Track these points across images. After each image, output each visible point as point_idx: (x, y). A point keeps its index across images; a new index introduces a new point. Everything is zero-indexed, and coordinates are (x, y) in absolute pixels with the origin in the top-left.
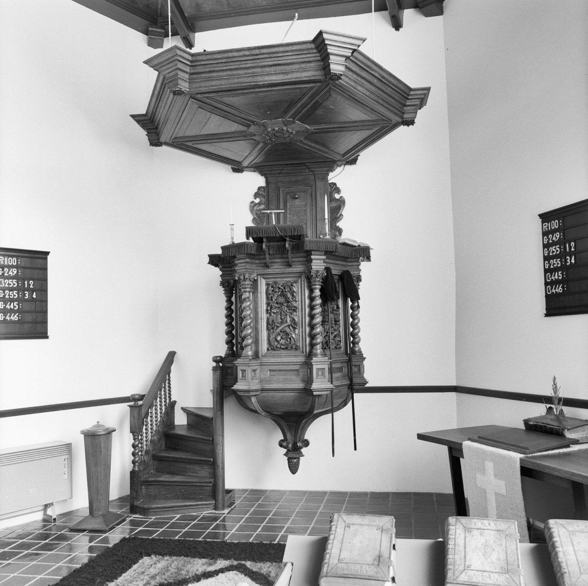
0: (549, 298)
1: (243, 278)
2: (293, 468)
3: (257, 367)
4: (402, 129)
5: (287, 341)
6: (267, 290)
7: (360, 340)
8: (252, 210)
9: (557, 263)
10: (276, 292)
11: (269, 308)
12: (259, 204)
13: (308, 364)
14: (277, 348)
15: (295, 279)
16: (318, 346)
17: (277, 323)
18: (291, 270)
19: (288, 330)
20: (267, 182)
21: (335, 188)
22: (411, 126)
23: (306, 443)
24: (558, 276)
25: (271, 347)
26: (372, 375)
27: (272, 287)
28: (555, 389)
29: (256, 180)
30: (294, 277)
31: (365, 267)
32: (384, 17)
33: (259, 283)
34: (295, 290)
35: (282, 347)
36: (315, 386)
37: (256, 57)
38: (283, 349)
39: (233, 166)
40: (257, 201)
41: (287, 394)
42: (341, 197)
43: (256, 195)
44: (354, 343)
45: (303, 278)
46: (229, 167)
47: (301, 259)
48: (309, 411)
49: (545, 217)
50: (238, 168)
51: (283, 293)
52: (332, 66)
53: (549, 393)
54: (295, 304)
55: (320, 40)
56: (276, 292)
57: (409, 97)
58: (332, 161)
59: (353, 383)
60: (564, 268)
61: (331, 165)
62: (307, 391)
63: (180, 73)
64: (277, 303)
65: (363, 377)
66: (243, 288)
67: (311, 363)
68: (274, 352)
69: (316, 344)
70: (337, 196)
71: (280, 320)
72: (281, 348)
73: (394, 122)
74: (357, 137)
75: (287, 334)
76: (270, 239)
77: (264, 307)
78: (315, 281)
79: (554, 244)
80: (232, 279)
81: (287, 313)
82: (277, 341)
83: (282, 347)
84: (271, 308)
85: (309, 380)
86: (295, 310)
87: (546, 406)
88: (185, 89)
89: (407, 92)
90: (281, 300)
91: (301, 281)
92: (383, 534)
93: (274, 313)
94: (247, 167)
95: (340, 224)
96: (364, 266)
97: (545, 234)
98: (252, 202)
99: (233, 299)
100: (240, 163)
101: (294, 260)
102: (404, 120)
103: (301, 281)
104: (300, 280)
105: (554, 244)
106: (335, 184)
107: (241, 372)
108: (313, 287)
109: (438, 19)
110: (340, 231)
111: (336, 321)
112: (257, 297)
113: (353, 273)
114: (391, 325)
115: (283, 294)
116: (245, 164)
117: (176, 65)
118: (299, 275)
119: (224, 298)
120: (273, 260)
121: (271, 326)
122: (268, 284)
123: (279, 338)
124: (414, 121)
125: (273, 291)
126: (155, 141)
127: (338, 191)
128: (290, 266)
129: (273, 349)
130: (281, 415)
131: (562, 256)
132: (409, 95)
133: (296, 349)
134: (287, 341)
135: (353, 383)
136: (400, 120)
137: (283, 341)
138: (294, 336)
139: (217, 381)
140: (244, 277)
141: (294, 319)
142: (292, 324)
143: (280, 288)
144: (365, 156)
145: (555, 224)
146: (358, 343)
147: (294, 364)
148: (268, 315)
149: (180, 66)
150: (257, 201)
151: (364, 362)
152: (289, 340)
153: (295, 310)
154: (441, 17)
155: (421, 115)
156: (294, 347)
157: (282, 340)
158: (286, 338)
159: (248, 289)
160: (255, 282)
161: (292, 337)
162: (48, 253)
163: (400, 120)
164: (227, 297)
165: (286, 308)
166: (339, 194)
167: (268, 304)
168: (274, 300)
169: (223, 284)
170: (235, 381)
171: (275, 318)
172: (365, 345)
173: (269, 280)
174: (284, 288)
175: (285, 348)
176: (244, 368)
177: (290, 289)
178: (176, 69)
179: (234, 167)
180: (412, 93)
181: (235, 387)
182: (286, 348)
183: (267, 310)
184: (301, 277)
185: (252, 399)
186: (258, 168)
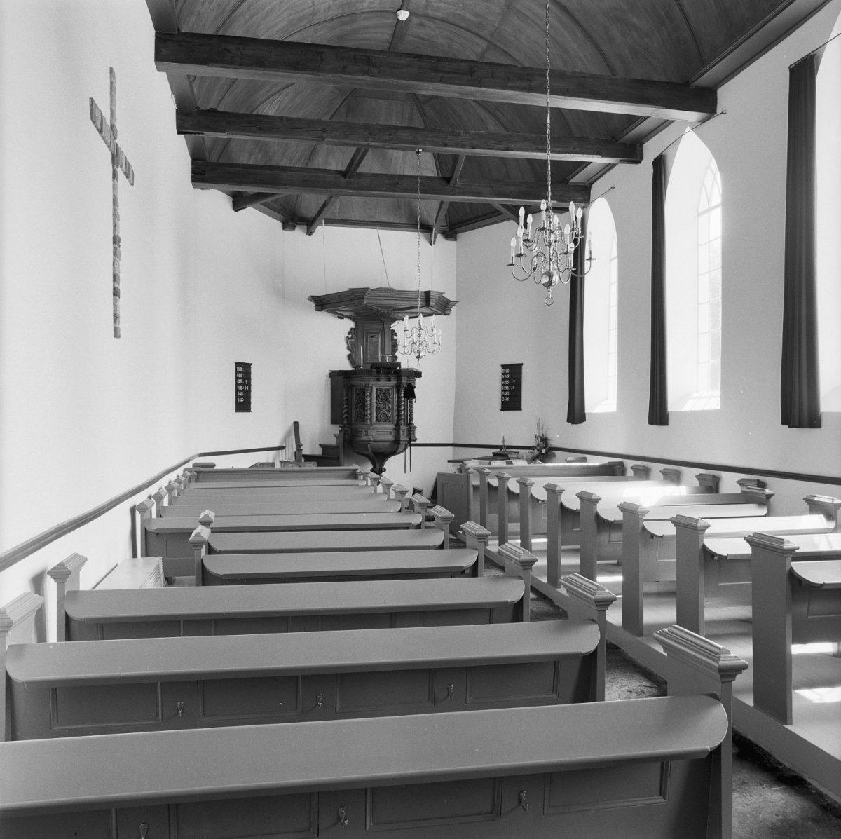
0: (503, 403)
8: (347, 342)
9: (507, 388)
12: (352, 338)
20: (356, 326)
24: (507, 393)
25: (378, 420)
26: (420, 436)
28: (504, 441)
29: (351, 324)
32: (425, 236)
40: (350, 336)
41: (385, 443)
43: (349, 333)
49: (504, 367)
53: (500, 443)
59: (411, 442)
60: (510, 390)
61: (394, 320)
70: (395, 338)
79: (507, 379)
86: (390, 402)
96: (418, 380)
97: (503, 374)
98: (347, 337)
105: (507, 379)
106: (393, 331)
109: (453, 243)
110: (396, 358)
113: (413, 384)
114: (430, 413)
115: (385, 395)
122: (377, 389)
127: (396, 335)
131: (510, 385)
135: (411, 442)
145: (508, 371)
147: (390, 428)
150: (350, 336)
153: (390, 402)
154: (455, 242)
162: (251, 364)
167: (377, 399)
172: (415, 421)
181: (362, 439)
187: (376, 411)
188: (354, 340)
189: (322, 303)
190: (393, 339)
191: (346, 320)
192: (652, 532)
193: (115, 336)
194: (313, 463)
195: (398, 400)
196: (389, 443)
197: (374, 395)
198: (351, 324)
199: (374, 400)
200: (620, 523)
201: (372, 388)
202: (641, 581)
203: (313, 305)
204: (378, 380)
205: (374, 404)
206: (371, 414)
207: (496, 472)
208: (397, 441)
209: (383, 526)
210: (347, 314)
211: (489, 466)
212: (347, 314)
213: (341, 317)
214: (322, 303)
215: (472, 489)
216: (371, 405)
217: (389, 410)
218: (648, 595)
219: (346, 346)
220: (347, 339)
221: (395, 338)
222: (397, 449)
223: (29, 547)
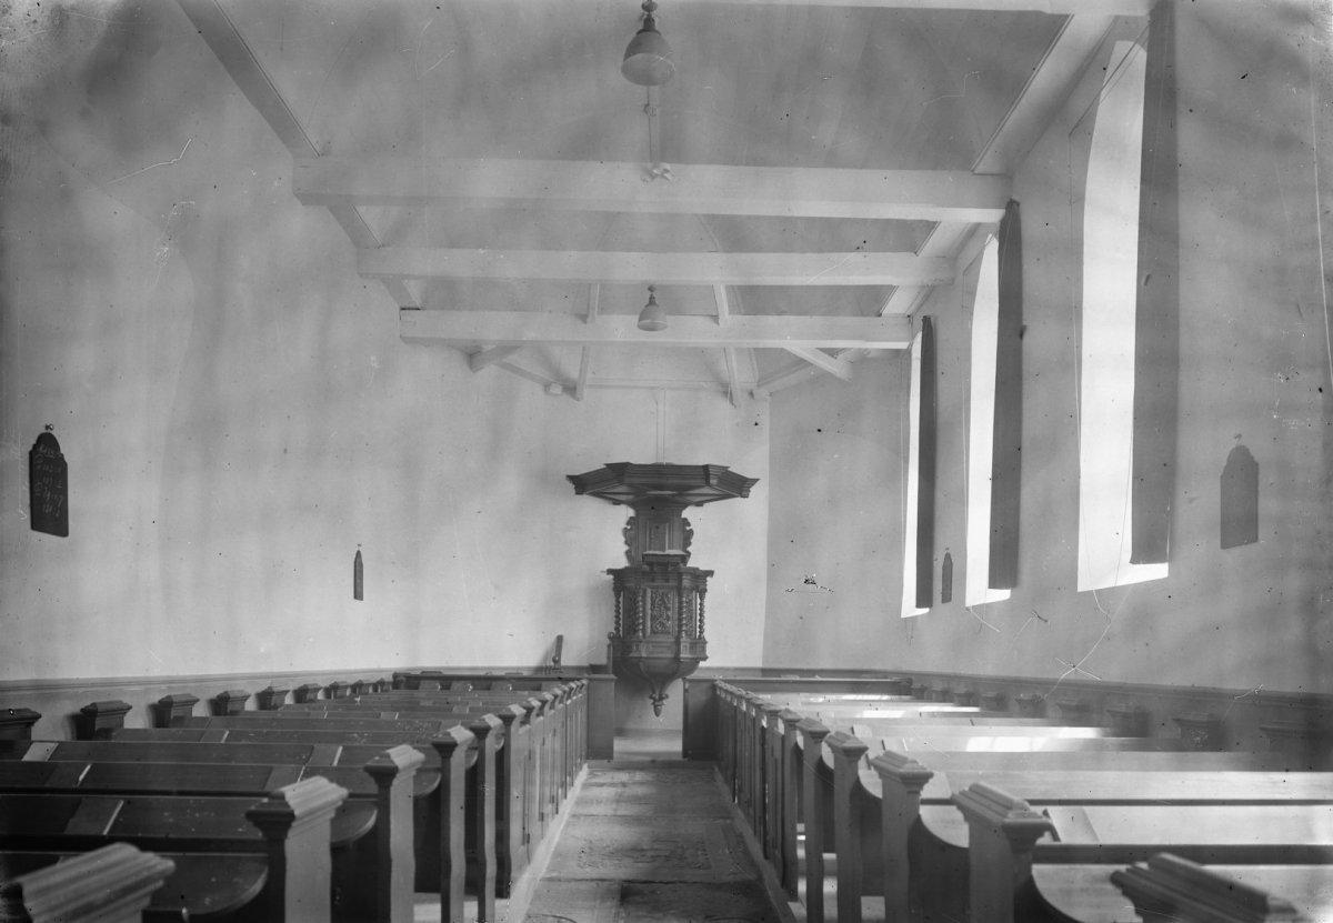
13: (678, 642)
20: (637, 511)
21: (686, 522)
23: (667, 697)
25: (653, 632)
29: (631, 512)
61: (685, 506)
62: (677, 659)
70: (688, 528)
76: (659, 564)
85: (678, 652)
86: (668, 609)
87: (1055, 836)
92: (594, 884)
95: (689, 549)
99: (621, 599)
106: (686, 519)
115: (662, 600)
119: (614, 599)
127: (689, 524)
128: (667, 581)
130: (32, 724)
139: (1193, 686)
153: (668, 609)
155: (754, 490)
169: (614, 589)
181: (631, 655)
186: (631, 504)
188: (632, 533)
189: (583, 484)
190: (684, 530)
191: (623, 507)
192: (701, 464)
193: (355, 597)
198: (631, 512)
199: (649, 606)
200: (423, 896)
201: (645, 591)
203: (571, 487)
204: (653, 580)
206: (644, 624)
210: (623, 498)
212: (623, 498)
213: (617, 503)
214: (583, 484)
215: (265, 714)
216: (644, 611)
217: (668, 618)
219: (623, 539)
221: (688, 528)
223: (867, 683)
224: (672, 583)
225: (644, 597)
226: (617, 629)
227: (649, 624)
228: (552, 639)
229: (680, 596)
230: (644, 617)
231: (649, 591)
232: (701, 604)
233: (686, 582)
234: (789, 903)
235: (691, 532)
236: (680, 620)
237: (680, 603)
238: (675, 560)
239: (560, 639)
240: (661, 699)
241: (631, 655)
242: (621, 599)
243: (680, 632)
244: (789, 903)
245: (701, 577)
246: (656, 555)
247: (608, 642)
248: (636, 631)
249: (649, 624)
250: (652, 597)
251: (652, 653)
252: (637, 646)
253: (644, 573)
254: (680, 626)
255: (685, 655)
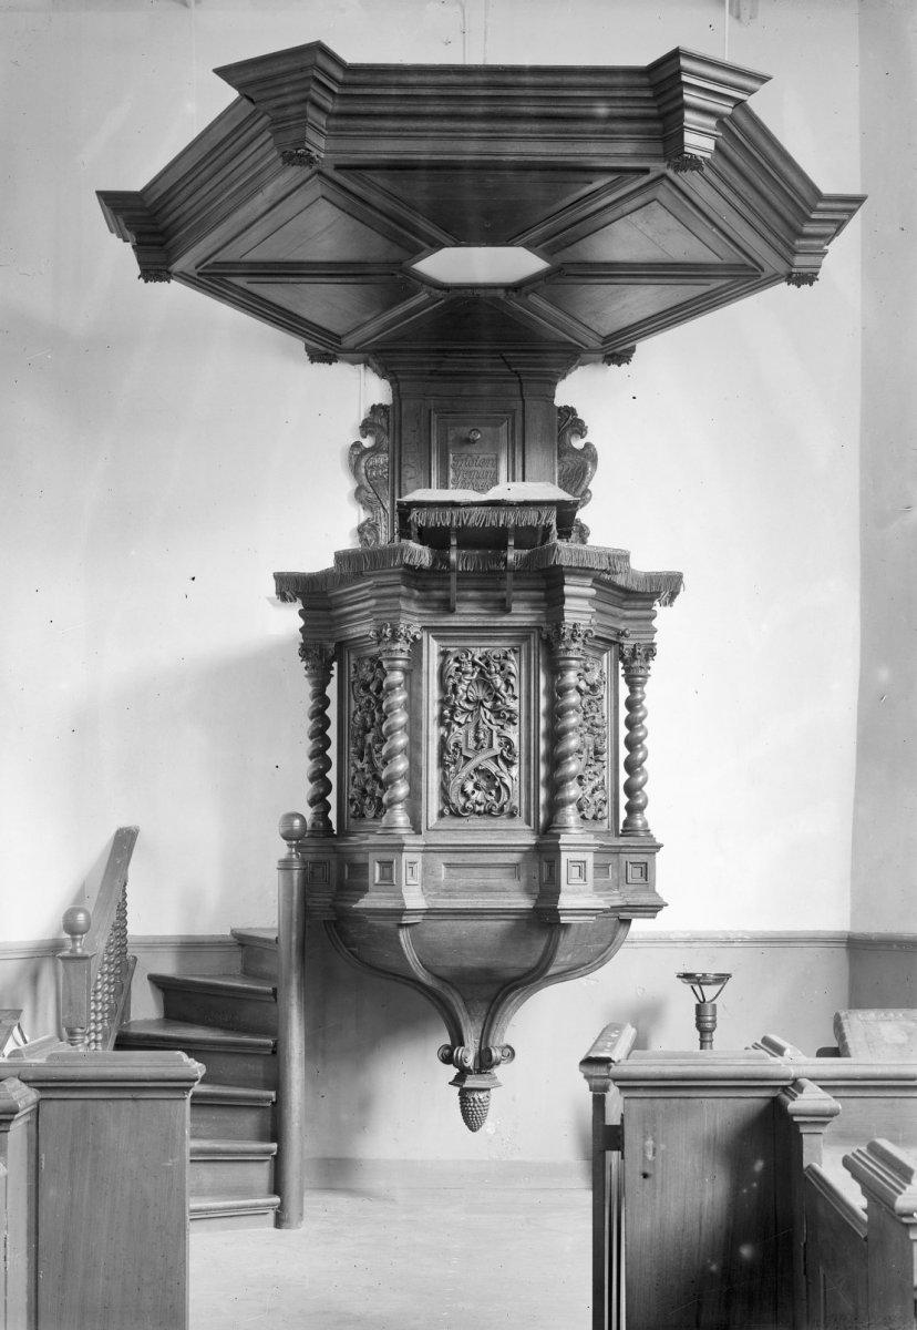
1: (389, 634)
2: (471, 1116)
3: (416, 855)
4: (783, 289)
5: (490, 794)
6: (442, 667)
7: (646, 801)
10: (465, 673)
11: (446, 712)
12: (375, 450)
13: (545, 853)
14: (465, 809)
15: (512, 643)
16: (571, 807)
17: (468, 749)
18: (505, 620)
19: (493, 769)
20: (397, 394)
21: (569, 421)
22: (805, 287)
27: (457, 660)
29: (376, 390)
30: (510, 638)
31: (665, 618)
33: (425, 648)
34: (513, 670)
35: (478, 808)
36: (566, 901)
37: (505, 93)
38: (479, 813)
39: (311, 343)
40: (368, 442)
42: (588, 445)
43: (366, 427)
44: (632, 809)
45: (534, 641)
46: (298, 345)
47: (532, 594)
48: (537, 967)
50: (326, 347)
51: (484, 677)
52: (689, 138)
54: (514, 705)
55: (667, 72)
56: (465, 673)
57: (814, 216)
58: (570, 351)
61: (571, 355)
63: (311, 111)
64: (468, 700)
65: (654, 892)
66: (389, 659)
67: (558, 845)
68: (457, 821)
69: (563, 803)
70: (578, 444)
71: (472, 744)
72: (473, 811)
73: (769, 271)
74: (639, 301)
75: (490, 777)
76: (472, 538)
77: (434, 710)
78: (568, 649)
80: (330, 640)
81: (491, 727)
82: (464, 792)
83: (478, 808)
84: (453, 712)
88: (318, 152)
89: (809, 201)
90: (480, 693)
91: (529, 649)
93: (459, 724)
94: (352, 351)
98: (357, 445)
99: (332, 691)
100: (338, 338)
101: (514, 594)
102: (794, 270)
103: (529, 649)
104: (524, 646)
106: (570, 411)
107: (377, 867)
108: (562, 663)
111: (597, 752)
112: (420, 684)
116: (349, 342)
117: (308, 89)
118: (523, 634)
119: (306, 688)
120: (463, 593)
121: (448, 755)
122: (444, 654)
123: (469, 787)
124: (816, 274)
125: (458, 669)
126: (155, 266)
127: (579, 428)
128: (506, 610)
129: (456, 814)
132: (813, 210)
133: (512, 815)
134: (490, 794)
136: (782, 268)
137: (478, 796)
138: (507, 781)
140: (394, 631)
141: (509, 742)
142: (505, 754)
143: (474, 664)
144: (648, 350)
146: (641, 809)
148: (443, 730)
149: (317, 94)
150: (368, 442)
151: (657, 854)
152: (493, 792)
156: (507, 808)
157: (477, 792)
158: (489, 788)
159: (400, 663)
160: (416, 644)
161: (505, 786)
163: (782, 268)
164: (314, 684)
165: (488, 714)
166: (582, 437)
167: (444, 702)
168: (461, 692)
169: (305, 652)
170: (364, 889)
171: (461, 738)
173: (448, 644)
174: (487, 664)
175: (485, 812)
176: (387, 856)
177: (502, 668)
178: (305, 101)
179: (314, 345)
180: (820, 205)
181: (365, 903)
182: (488, 813)
183: (441, 718)
184: (527, 638)
185: (401, 935)
187: (442, 764)
188: (392, 443)
194: (561, 939)
195: (552, 702)
196: (498, 925)
197: (432, 692)
198: (376, 390)
202: (187, 1194)
205: (433, 733)
206: (414, 776)
207: (17, 1071)
208: (544, 919)
209: (33, 1193)
211: (832, 1066)
218: (205, 1215)
219: (348, 485)
220: (357, 454)
221: (578, 444)
222: (548, 958)
224: (522, 615)
225: (413, 670)
226: (319, 801)
227: (433, 776)
228: (104, 839)
229: (556, 669)
230: (414, 748)
231: (432, 648)
232: (631, 704)
233: (579, 606)
234: (415, 266)
235: (589, 454)
236: (556, 761)
237: (557, 692)
238: (531, 517)
239: (125, 842)
240: (485, 1062)
241: (365, 903)
242: (332, 691)
243: (555, 806)
244: (415, 266)
245: (632, 596)
246: (454, 505)
247: (282, 849)
248: (381, 808)
249: (433, 776)
250: (442, 675)
251: (449, 891)
252: (387, 865)
253: (413, 575)
254: (555, 785)
255: (577, 895)
